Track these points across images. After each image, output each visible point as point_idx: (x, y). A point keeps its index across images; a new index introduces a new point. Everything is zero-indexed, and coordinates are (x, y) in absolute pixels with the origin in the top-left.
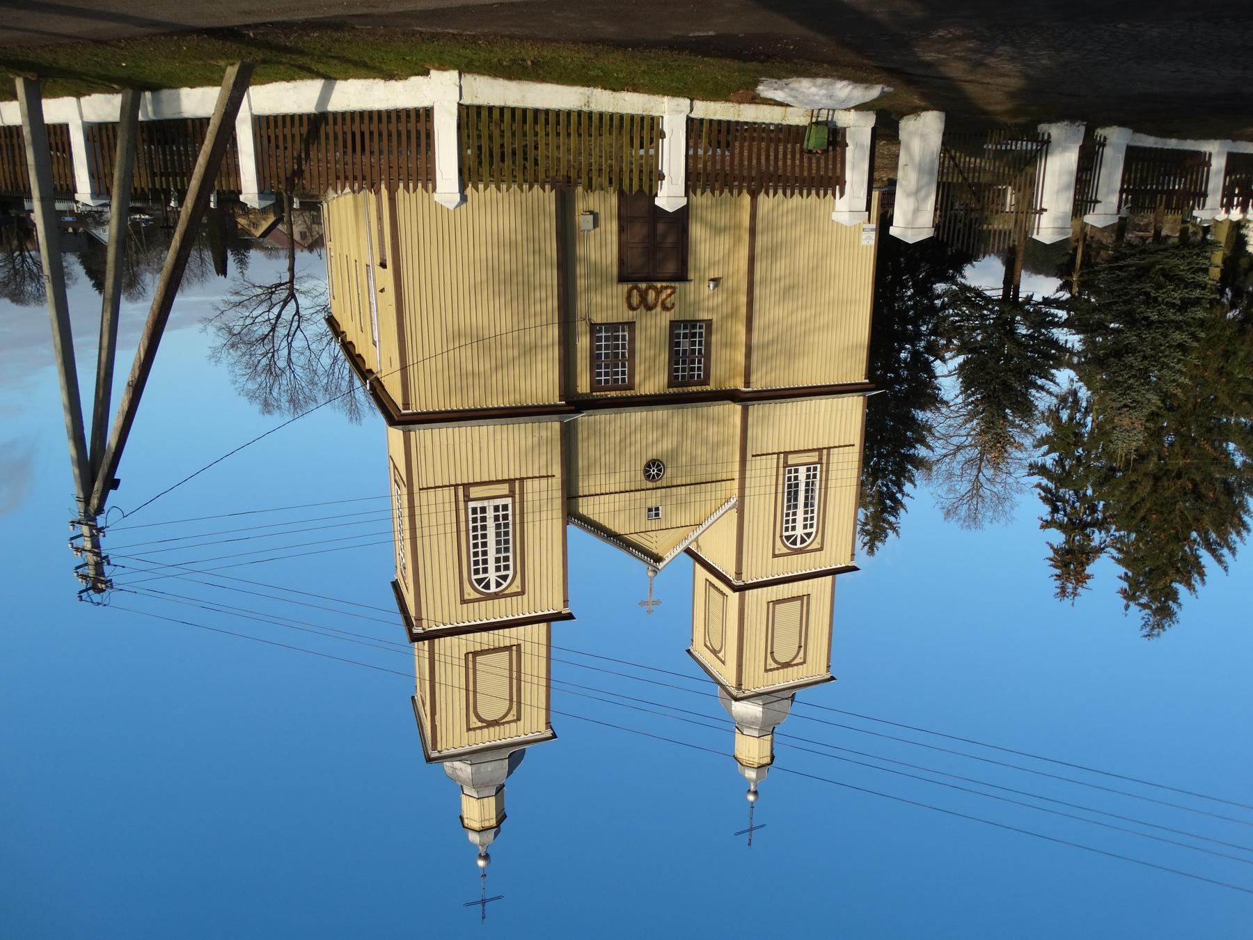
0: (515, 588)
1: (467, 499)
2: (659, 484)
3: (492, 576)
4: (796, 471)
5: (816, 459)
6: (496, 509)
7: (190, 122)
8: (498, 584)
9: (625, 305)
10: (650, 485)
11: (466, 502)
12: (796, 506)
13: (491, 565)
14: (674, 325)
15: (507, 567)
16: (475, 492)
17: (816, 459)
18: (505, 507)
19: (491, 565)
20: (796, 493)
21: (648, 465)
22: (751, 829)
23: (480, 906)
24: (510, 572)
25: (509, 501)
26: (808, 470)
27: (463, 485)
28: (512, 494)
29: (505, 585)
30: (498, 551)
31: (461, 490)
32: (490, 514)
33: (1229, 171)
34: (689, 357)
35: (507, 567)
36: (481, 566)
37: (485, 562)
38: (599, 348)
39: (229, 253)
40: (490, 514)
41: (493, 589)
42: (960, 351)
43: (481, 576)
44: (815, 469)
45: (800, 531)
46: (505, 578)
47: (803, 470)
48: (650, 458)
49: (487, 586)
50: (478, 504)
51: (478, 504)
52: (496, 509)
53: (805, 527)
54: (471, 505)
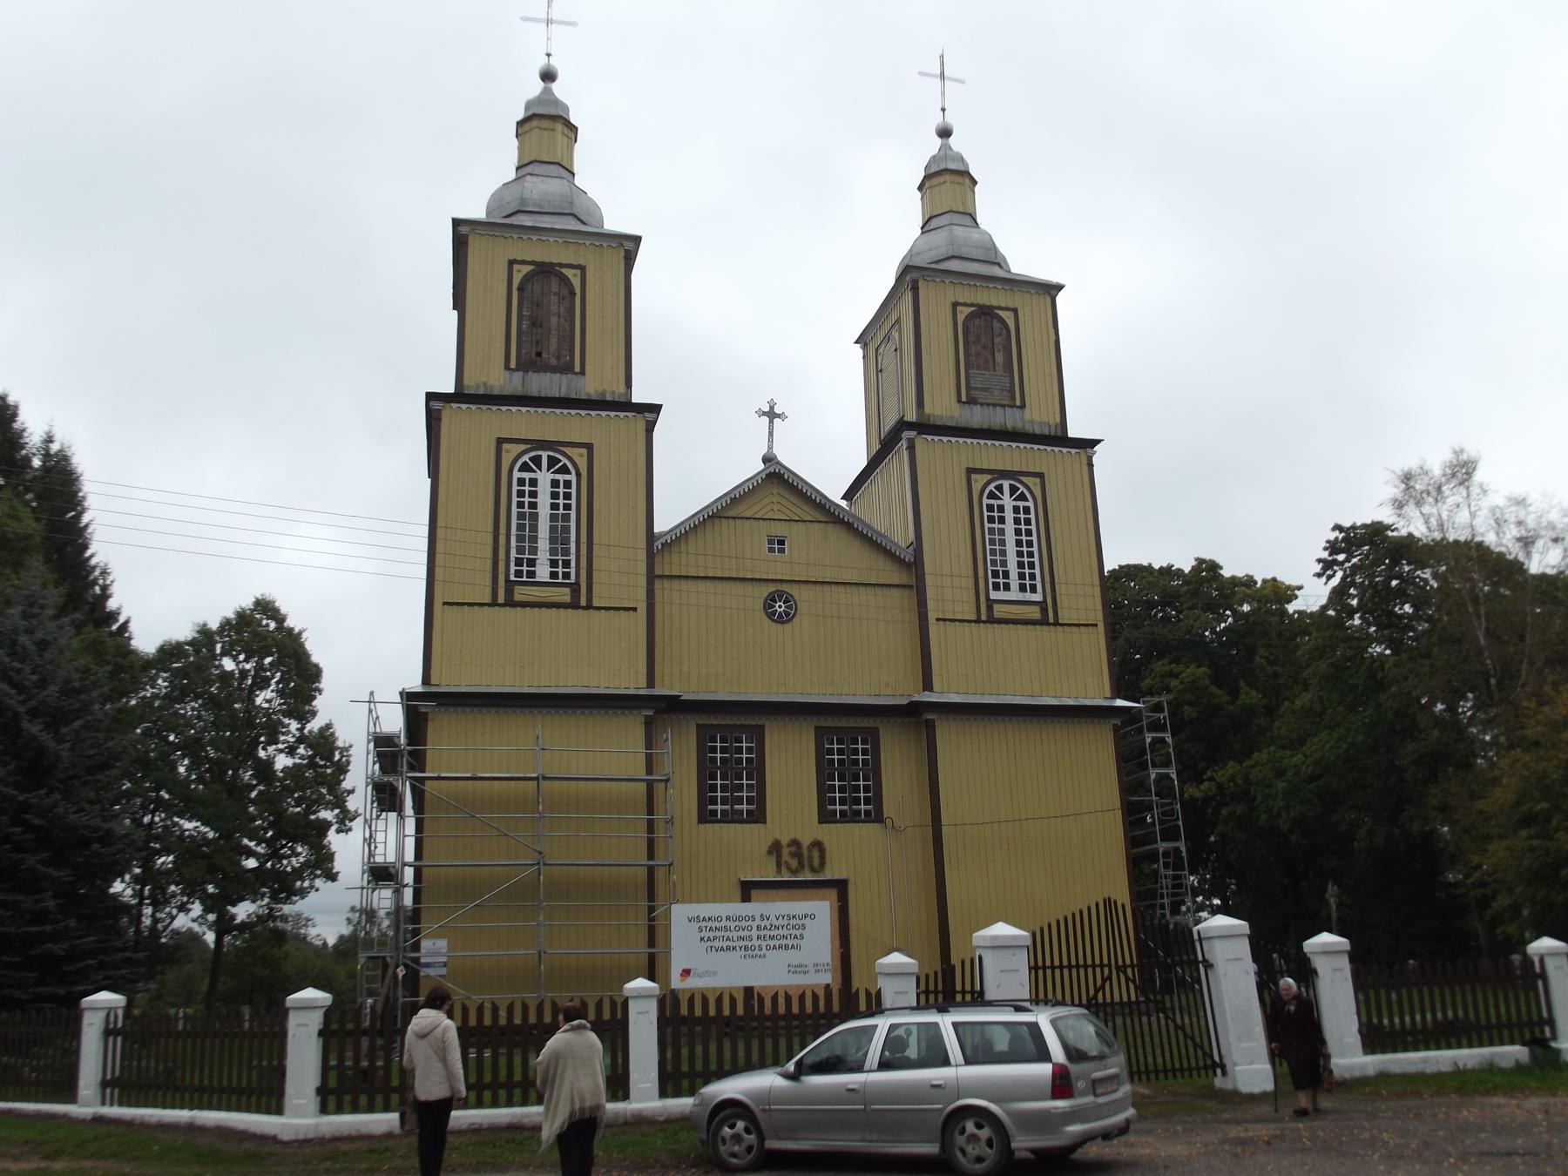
0: (579, 455)
1: (1042, 605)
2: (772, 588)
3: (1008, 501)
4: (554, 575)
5: (518, 589)
6: (1007, 587)
7: (1506, 1039)
8: (999, 488)
9: (827, 846)
10: (785, 587)
11: (1045, 601)
12: (553, 518)
13: (1009, 515)
14: (758, 816)
15: (521, 482)
16: (1034, 613)
17: (518, 589)
18: (996, 587)
19: (1009, 515)
20: (553, 540)
21: (771, 616)
22: (549, 22)
23: (554, 27)
24: (516, 475)
25: (994, 595)
26: (532, 574)
27: (1048, 624)
28: (991, 603)
29: (992, 487)
30: (1002, 532)
31: (583, 602)
32: (1014, 582)
33: (339, 1110)
34: (848, 771)
35: (521, 482)
36: (561, 490)
37: (1017, 521)
38: (713, 788)
39: (212, 946)
40: (1014, 582)
41: (1006, 485)
42: (183, 757)
43: (1021, 504)
44: (519, 574)
45: (544, 478)
46: (525, 468)
47: (543, 572)
48: (787, 627)
49: (552, 462)
50: (1029, 596)
51: (1029, 596)
52: (1007, 587)
53: (534, 482)
54: (1037, 597)
